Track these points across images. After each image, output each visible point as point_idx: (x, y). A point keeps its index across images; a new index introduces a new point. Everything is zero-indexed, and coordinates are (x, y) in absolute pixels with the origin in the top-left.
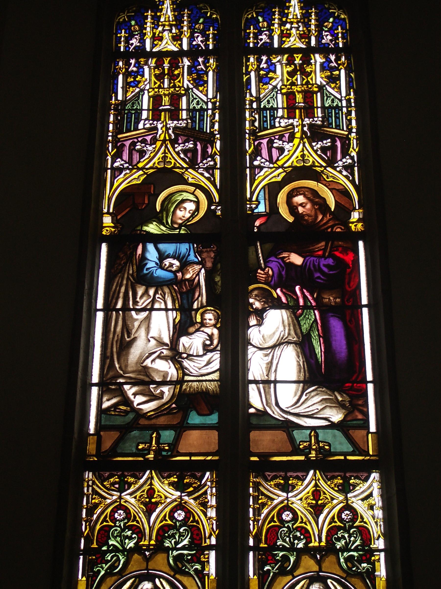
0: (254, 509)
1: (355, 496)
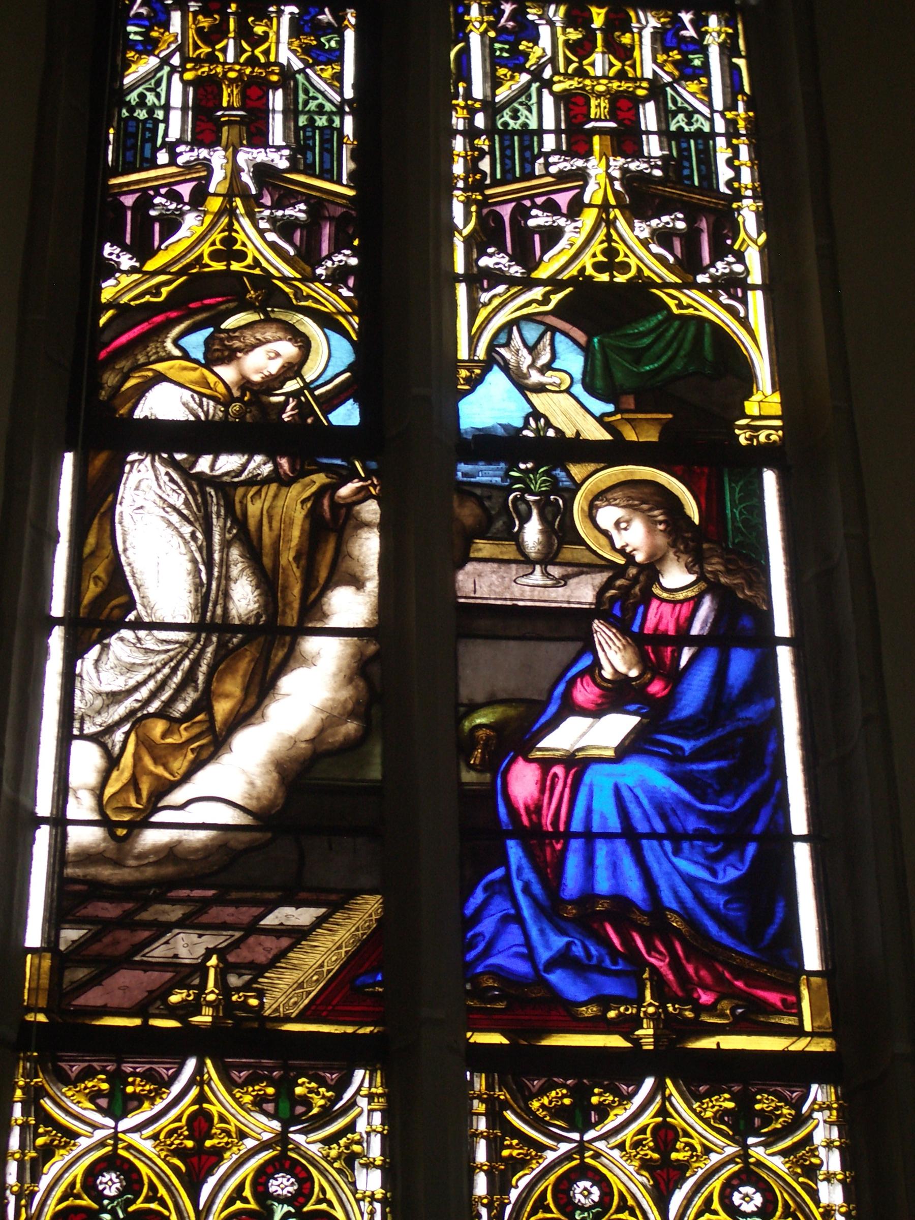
0: (21, 1163)
1: (605, 1137)
